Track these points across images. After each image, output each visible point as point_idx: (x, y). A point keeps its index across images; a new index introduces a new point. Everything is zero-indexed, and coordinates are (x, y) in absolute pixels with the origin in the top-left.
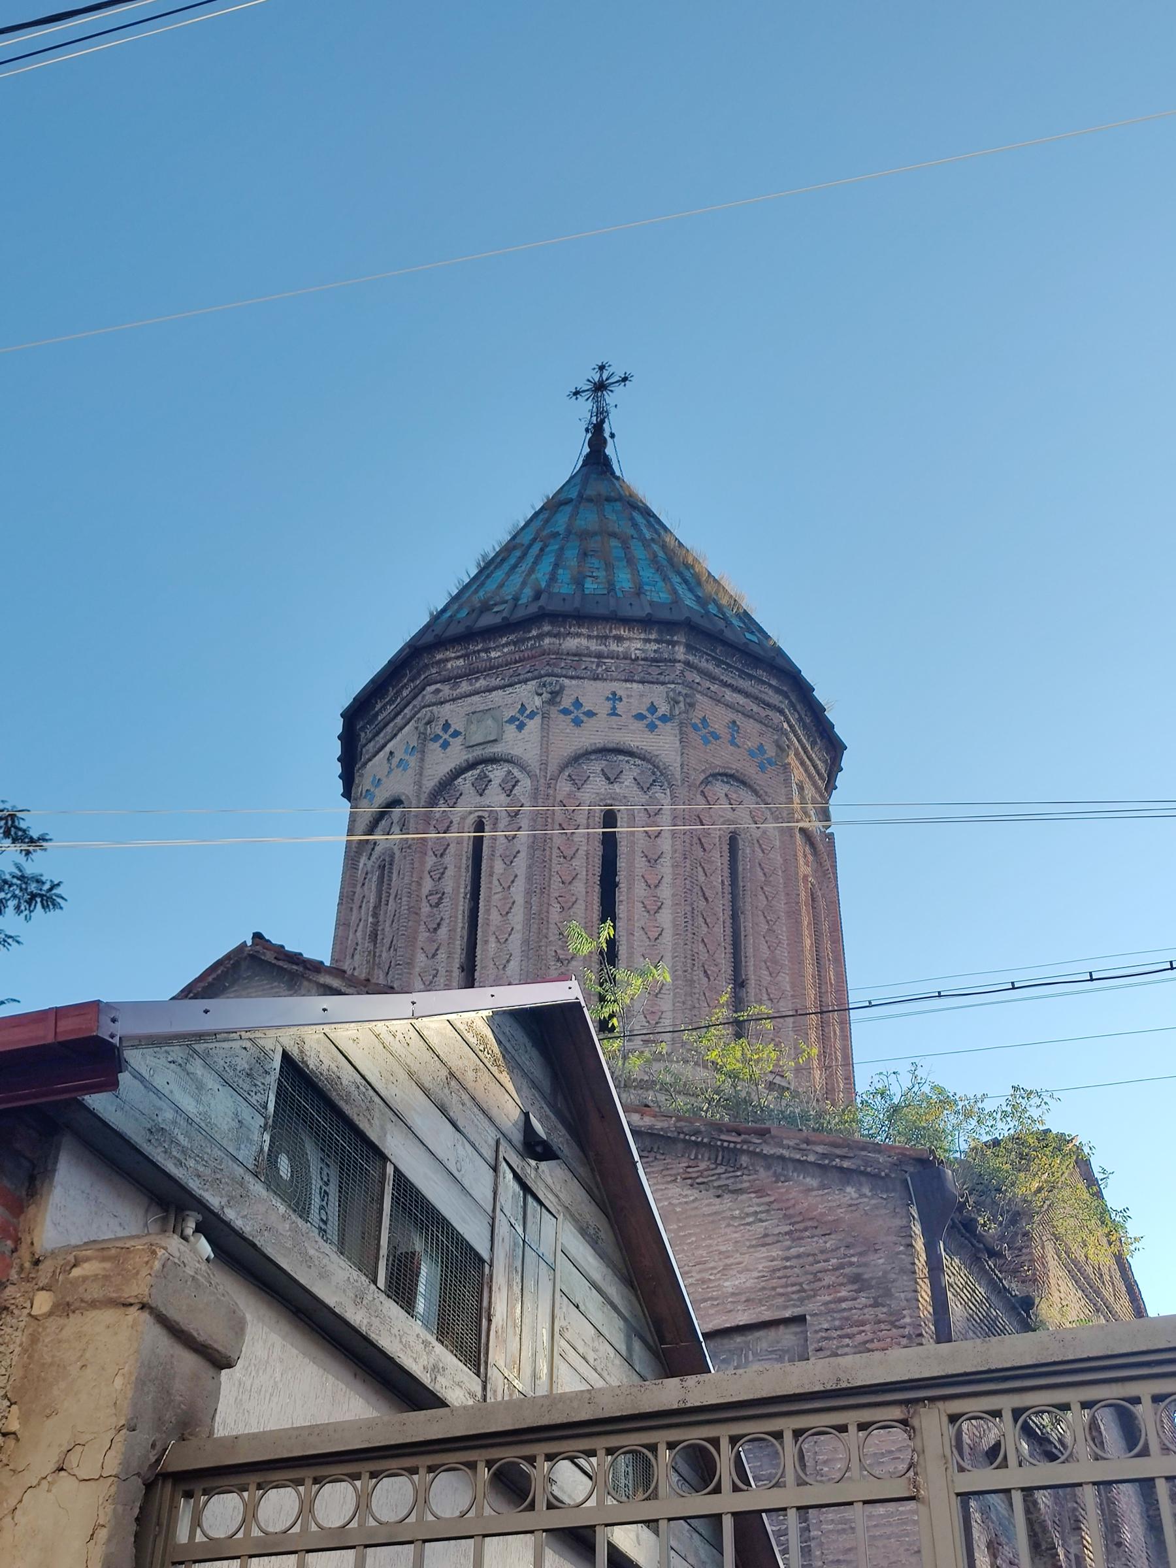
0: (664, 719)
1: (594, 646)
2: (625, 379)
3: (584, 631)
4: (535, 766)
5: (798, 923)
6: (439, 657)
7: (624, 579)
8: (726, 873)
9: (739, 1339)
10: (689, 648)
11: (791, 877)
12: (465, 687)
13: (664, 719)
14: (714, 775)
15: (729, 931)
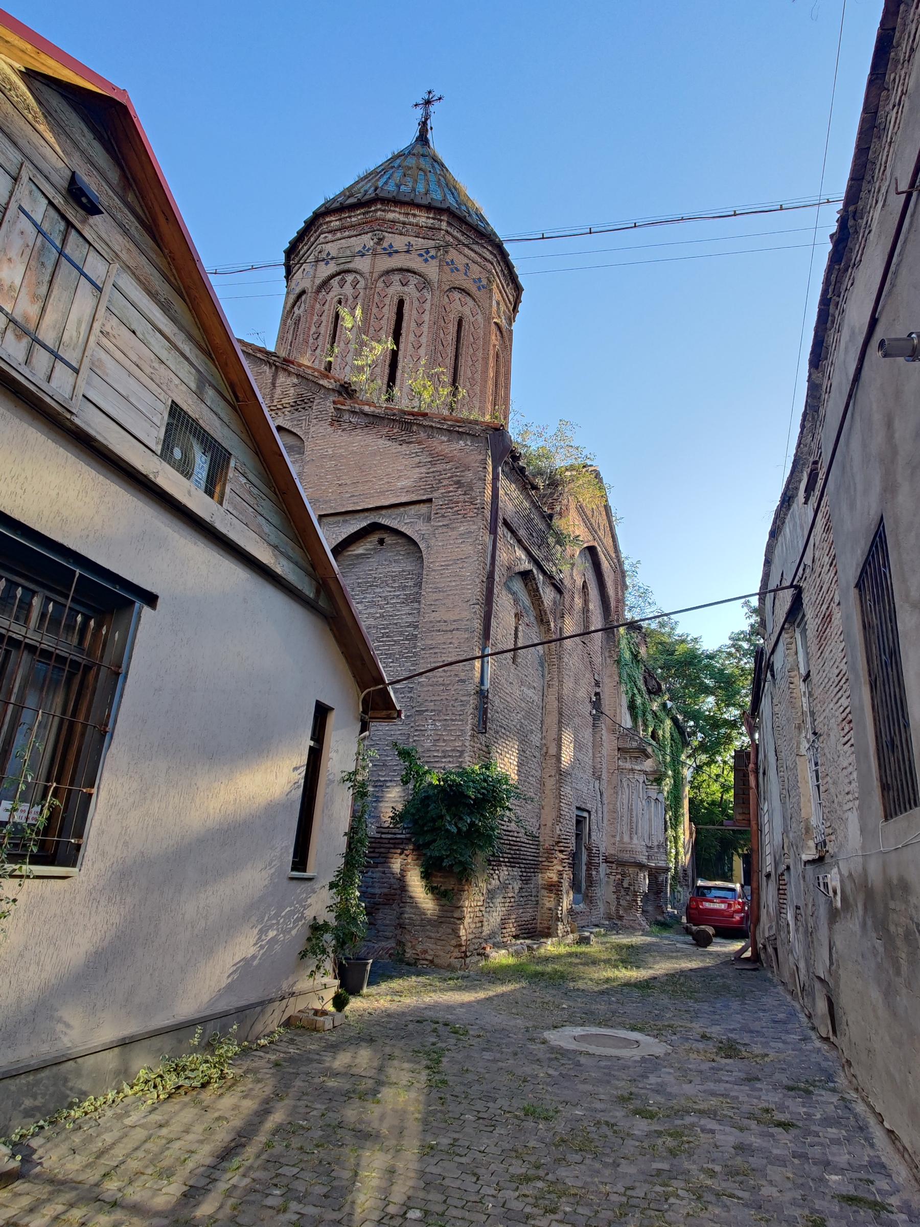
0: (432, 257)
1: (402, 218)
2: (440, 99)
3: (397, 209)
4: (367, 275)
5: (487, 363)
6: (328, 219)
7: (421, 188)
8: (455, 335)
9: (402, 509)
10: (449, 224)
11: (486, 342)
12: (339, 235)
13: (432, 257)
14: (454, 288)
15: (453, 362)
